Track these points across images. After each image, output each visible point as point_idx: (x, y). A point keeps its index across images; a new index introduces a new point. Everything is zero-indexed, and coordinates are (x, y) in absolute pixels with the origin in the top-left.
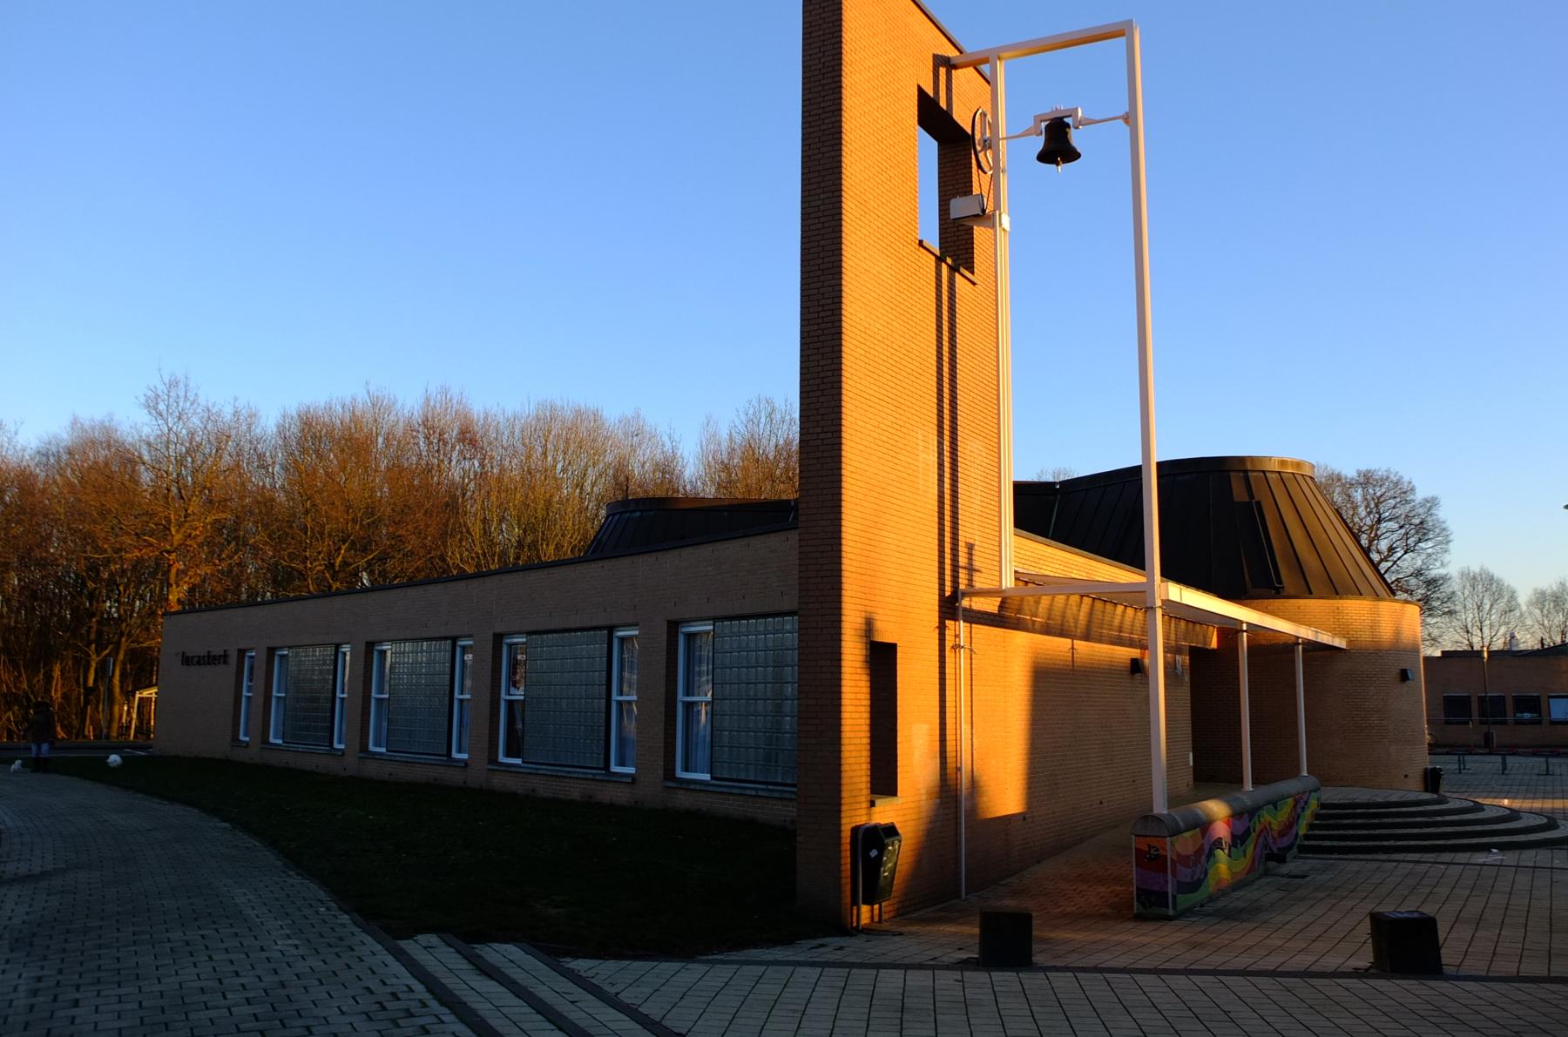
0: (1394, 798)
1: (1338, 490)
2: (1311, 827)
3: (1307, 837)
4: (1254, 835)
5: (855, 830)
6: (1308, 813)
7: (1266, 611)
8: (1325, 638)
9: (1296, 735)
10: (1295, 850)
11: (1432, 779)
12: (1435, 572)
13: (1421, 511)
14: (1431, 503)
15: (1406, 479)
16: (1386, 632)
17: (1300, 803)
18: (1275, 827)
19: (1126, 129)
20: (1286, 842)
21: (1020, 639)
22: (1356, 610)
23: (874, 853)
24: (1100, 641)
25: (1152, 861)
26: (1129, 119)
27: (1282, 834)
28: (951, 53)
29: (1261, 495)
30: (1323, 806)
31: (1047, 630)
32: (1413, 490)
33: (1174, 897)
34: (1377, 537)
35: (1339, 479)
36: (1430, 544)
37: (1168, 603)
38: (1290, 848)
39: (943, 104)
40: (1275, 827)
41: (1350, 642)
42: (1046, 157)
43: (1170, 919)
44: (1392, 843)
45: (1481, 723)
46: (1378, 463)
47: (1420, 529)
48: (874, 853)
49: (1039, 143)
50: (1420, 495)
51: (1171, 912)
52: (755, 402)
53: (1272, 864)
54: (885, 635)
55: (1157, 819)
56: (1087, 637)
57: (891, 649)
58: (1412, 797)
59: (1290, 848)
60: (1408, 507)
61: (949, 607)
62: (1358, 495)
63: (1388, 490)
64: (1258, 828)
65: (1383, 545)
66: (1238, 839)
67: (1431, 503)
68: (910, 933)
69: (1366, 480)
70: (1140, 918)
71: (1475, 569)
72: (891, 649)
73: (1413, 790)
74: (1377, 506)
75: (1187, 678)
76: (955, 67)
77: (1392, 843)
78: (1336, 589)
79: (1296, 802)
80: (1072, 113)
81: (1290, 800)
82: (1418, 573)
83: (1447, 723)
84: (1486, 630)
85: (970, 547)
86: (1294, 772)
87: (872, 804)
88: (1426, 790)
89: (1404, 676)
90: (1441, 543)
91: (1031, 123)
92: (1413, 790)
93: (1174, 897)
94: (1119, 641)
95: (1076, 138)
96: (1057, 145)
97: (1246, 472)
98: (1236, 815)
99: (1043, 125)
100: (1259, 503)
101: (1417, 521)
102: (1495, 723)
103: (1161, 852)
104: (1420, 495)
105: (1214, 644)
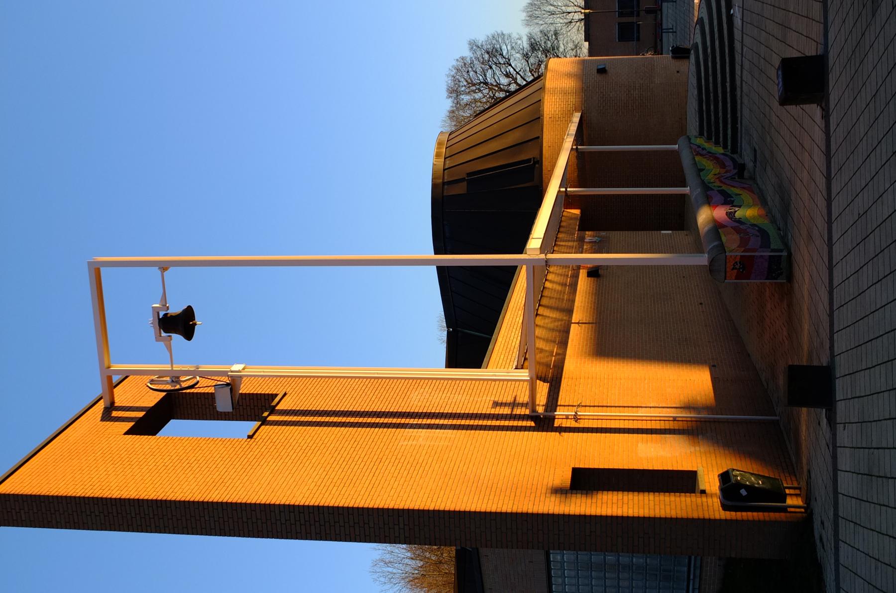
0: (693, 81)
1: (461, 113)
2: (717, 143)
3: (725, 147)
4: (724, 187)
5: (725, 507)
6: (706, 145)
7: (553, 165)
8: (573, 128)
9: (647, 153)
10: (735, 156)
11: (680, 53)
12: (526, 45)
13: (479, 53)
14: (474, 46)
15: (455, 63)
16: (569, 84)
17: (699, 151)
18: (718, 171)
19: (172, 269)
20: (729, 163)
21: (570, 365)
22: (551, 106)
23: (743, 492)
24: (573, 301)
25: (745, 268)
26: (164, 267)
27: (723, 166)
28: (101, 406)
29: (461, 173)
30: (701, 134)
31: (564, 343)
32: (463, 58)
33: (773, 250)
34: (498, 85)
35: (453, 112)
36: (504, 47)
37: (543, 249)
38: (733, 160)
39: (141, 414)
40: (718, 171)
41: (576, 110)
42: (189, 334)
43: (790, 255)
44: (728, 85)
45: (638, 15)
46: (442, 82)
47: (492, 54)
48: (743, 492)
49: (177, 339)
50: (467, 54)
51: (785, 254)
52: (375, 576)
53: (746, 174)
54: (564, 477)
55: (712, 262)
56: (570, 312)
57: (576, 472)
58: (693, 68)
59: (733, 160)
60: (476, 62)
61: (544, 423)
62: (466, 98)
63: (462, 76)
64: (718, 184)
65: (504, 81)
66: (728, 200)
67: (474, 46)
68: (809, 471)
69: (454, 92)
70: (790, 278)
71: (524, 16)
72: (576, 472)
73: (688, 67)
74: (474, 85)
75: (603, 233)
76: (113, 403)
77: (728, 85)
78: (536, 119)
79: (698, 154)
80: (156, 311)
81: (697, 158)
82: (526, 57)
83: (638, 39)
84: (569, 9)
85: (496, 404)
86: (676, 154)
87: (703, 492)
88: (688, 58)
89: (602, 71)
90: (503, 39)
91: (162, 343)
92: (688, 67)
93: (773, 250)
94: (574, 286)
95: (176, 309)
96: (181, 324)
97: (444, 183)
98: (709, 201)
99: (163, 334)
100: (469, 174)
101: (486, 56)
102: (638, 6)
103: (738, 260)
104: (467, 54)
105: (577, 212)
